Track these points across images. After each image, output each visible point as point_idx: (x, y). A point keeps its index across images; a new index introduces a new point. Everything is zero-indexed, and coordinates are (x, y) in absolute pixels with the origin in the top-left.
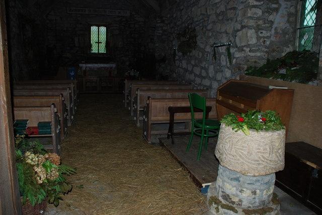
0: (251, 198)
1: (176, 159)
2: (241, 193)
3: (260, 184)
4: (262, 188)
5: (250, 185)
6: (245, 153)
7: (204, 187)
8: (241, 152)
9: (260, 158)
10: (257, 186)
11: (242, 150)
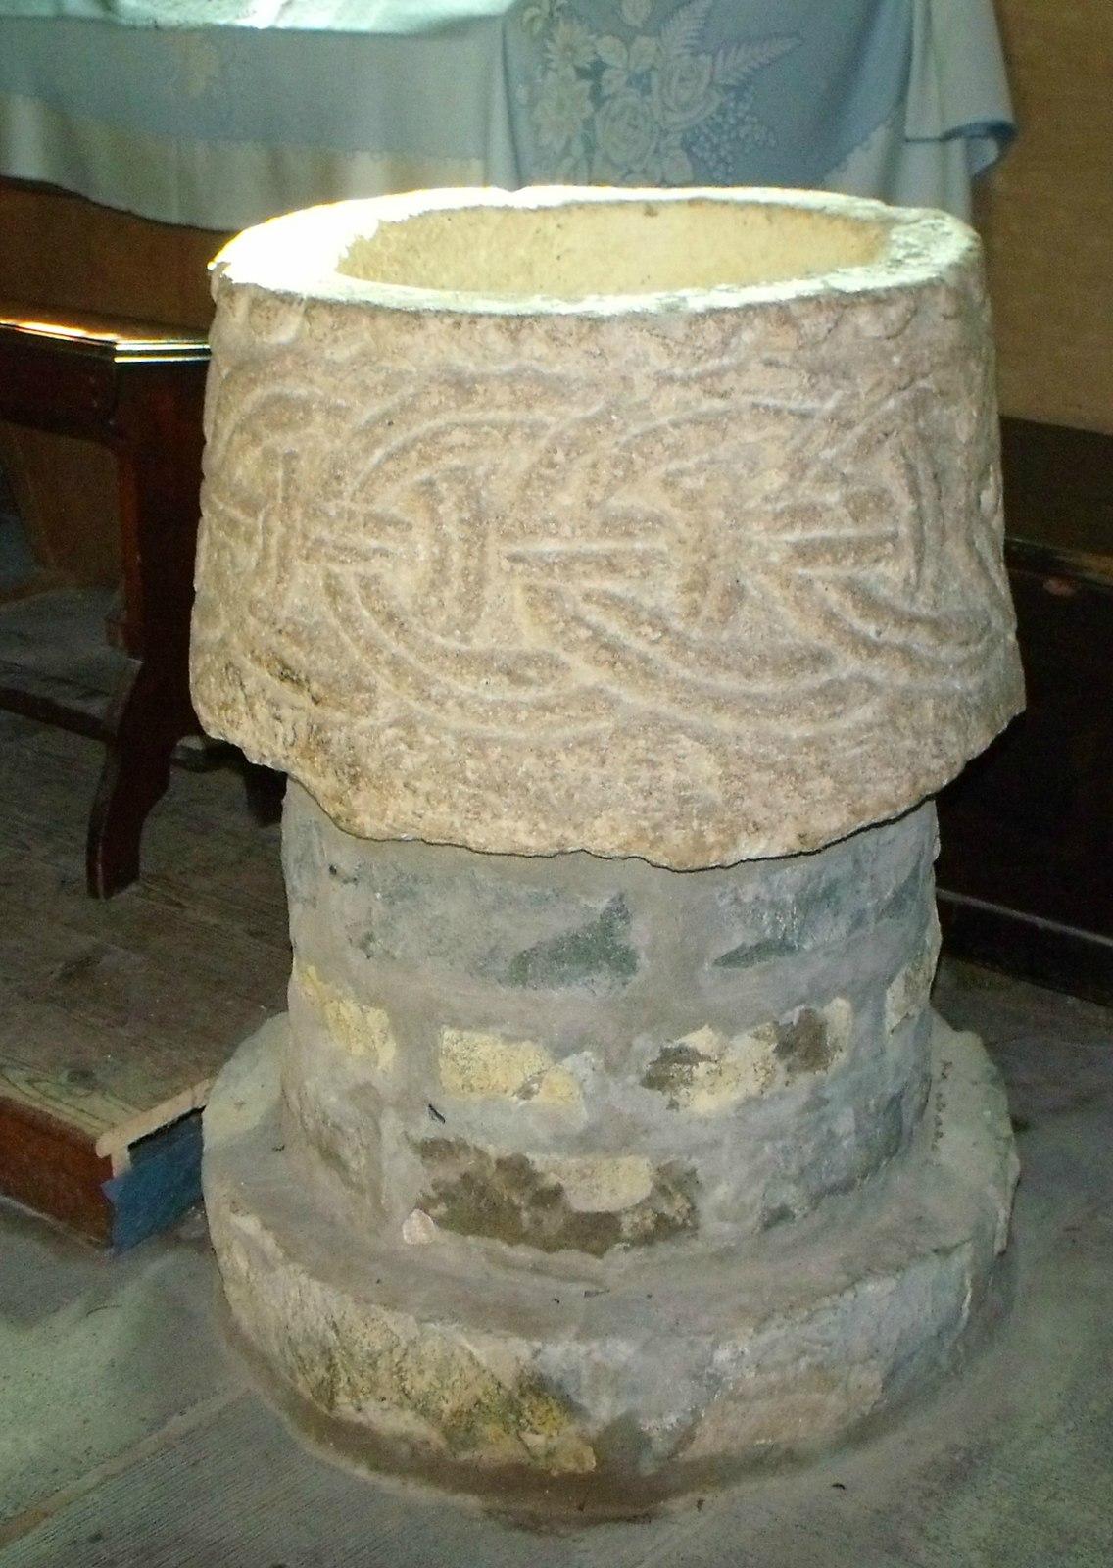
0: (786, 1111)
2: (660, 1098)
3: (842, 926)
5: (750, 976)
6: (667, 594)
9: (830, 618)
10: (822, 963)
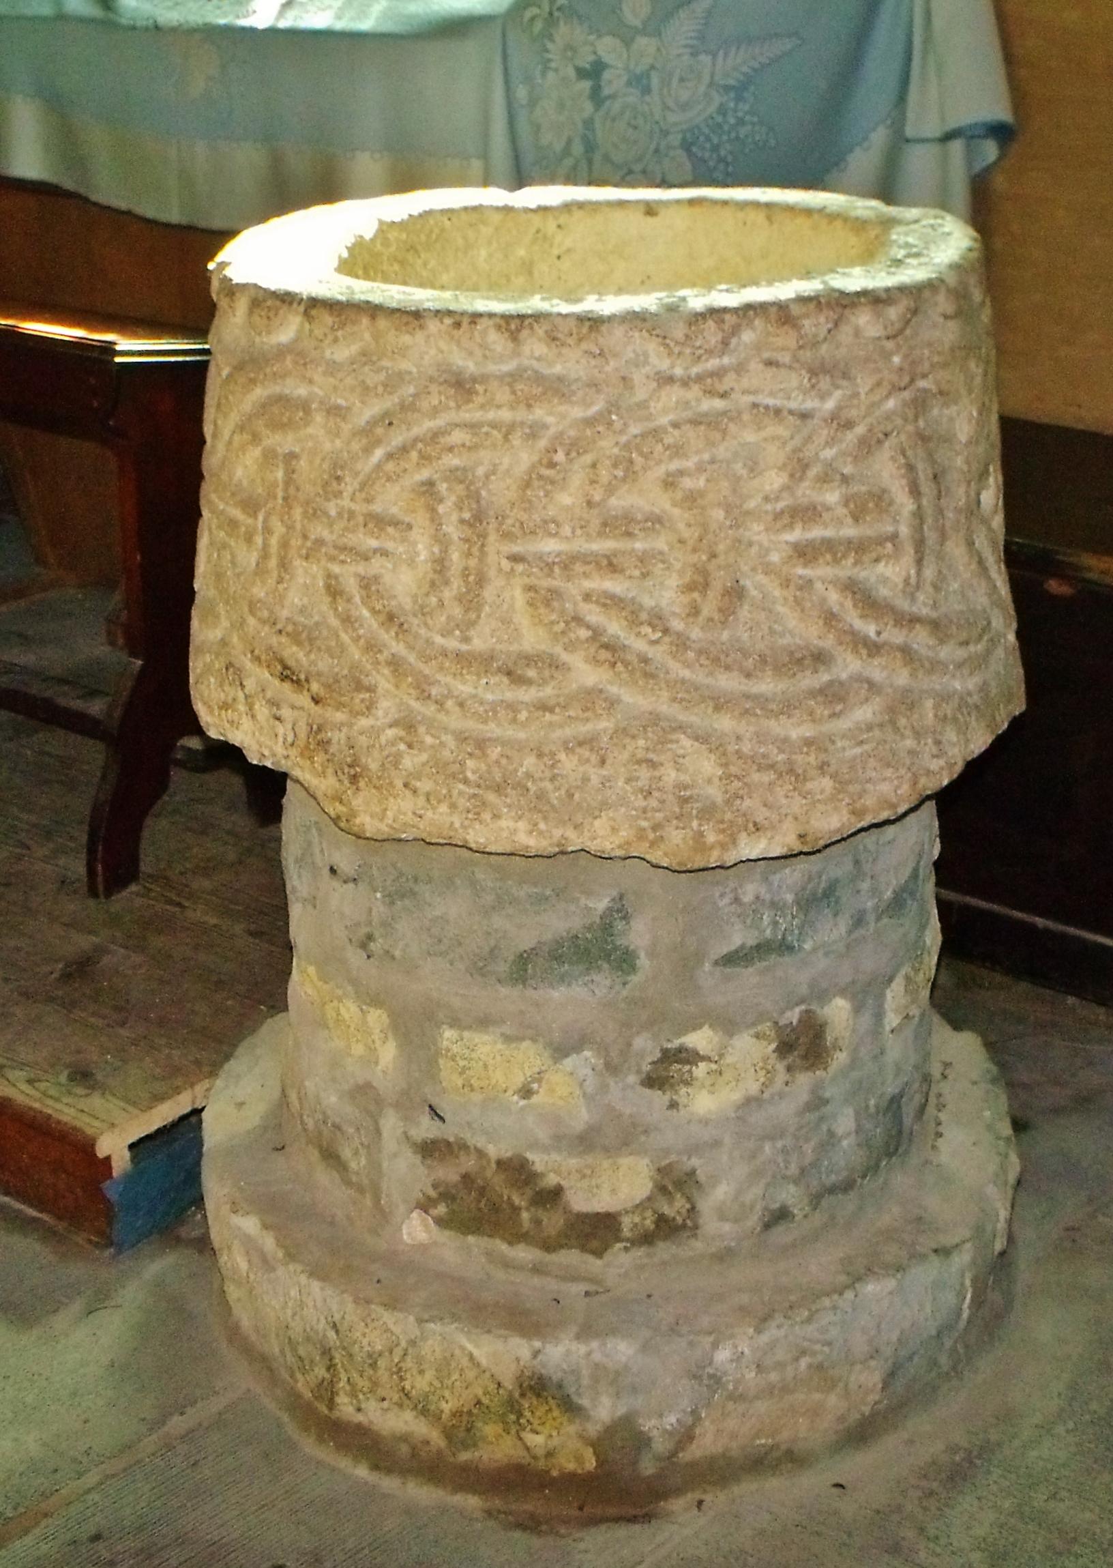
0: (786, 1110)
1: (306, 789)
2: (659, 1098)
3: (843, 924)
4: (871, 961)
5: (749, 975)
6: (666, 594)
7: (121, 1161)
8: (611, 602)
9: (830, 618)
10: (822, 963)
11: (611, 565)
